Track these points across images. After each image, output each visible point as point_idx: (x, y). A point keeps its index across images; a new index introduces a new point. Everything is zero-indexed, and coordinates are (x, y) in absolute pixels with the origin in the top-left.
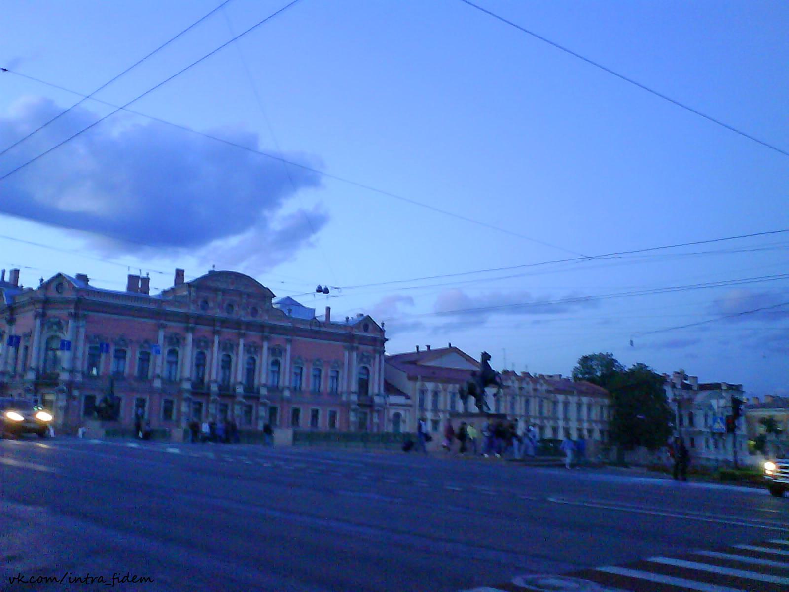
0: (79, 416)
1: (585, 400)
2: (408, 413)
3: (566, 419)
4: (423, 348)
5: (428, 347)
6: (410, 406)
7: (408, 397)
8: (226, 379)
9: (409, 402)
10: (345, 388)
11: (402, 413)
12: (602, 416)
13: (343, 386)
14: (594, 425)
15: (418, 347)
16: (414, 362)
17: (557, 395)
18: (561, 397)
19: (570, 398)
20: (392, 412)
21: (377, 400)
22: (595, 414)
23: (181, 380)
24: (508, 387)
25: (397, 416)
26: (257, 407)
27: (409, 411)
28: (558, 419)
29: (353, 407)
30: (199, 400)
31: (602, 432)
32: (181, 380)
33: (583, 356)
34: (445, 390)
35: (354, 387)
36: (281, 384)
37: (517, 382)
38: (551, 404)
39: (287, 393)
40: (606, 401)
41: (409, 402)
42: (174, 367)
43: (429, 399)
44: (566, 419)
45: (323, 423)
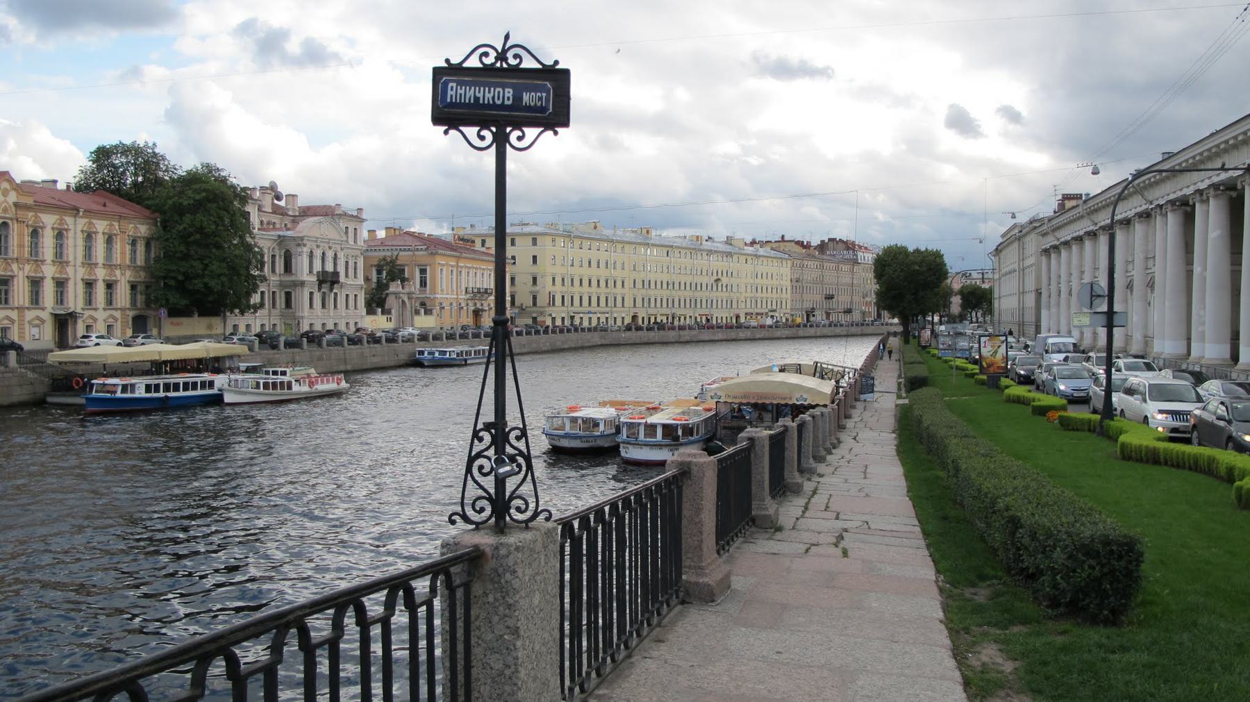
1: (101, 226)
12: (133, 259)
14: (118, 272)
18: (49, 220)
19: (69, 220)
22: (121, 251)
31: (133, 287)
40: (143, 230)
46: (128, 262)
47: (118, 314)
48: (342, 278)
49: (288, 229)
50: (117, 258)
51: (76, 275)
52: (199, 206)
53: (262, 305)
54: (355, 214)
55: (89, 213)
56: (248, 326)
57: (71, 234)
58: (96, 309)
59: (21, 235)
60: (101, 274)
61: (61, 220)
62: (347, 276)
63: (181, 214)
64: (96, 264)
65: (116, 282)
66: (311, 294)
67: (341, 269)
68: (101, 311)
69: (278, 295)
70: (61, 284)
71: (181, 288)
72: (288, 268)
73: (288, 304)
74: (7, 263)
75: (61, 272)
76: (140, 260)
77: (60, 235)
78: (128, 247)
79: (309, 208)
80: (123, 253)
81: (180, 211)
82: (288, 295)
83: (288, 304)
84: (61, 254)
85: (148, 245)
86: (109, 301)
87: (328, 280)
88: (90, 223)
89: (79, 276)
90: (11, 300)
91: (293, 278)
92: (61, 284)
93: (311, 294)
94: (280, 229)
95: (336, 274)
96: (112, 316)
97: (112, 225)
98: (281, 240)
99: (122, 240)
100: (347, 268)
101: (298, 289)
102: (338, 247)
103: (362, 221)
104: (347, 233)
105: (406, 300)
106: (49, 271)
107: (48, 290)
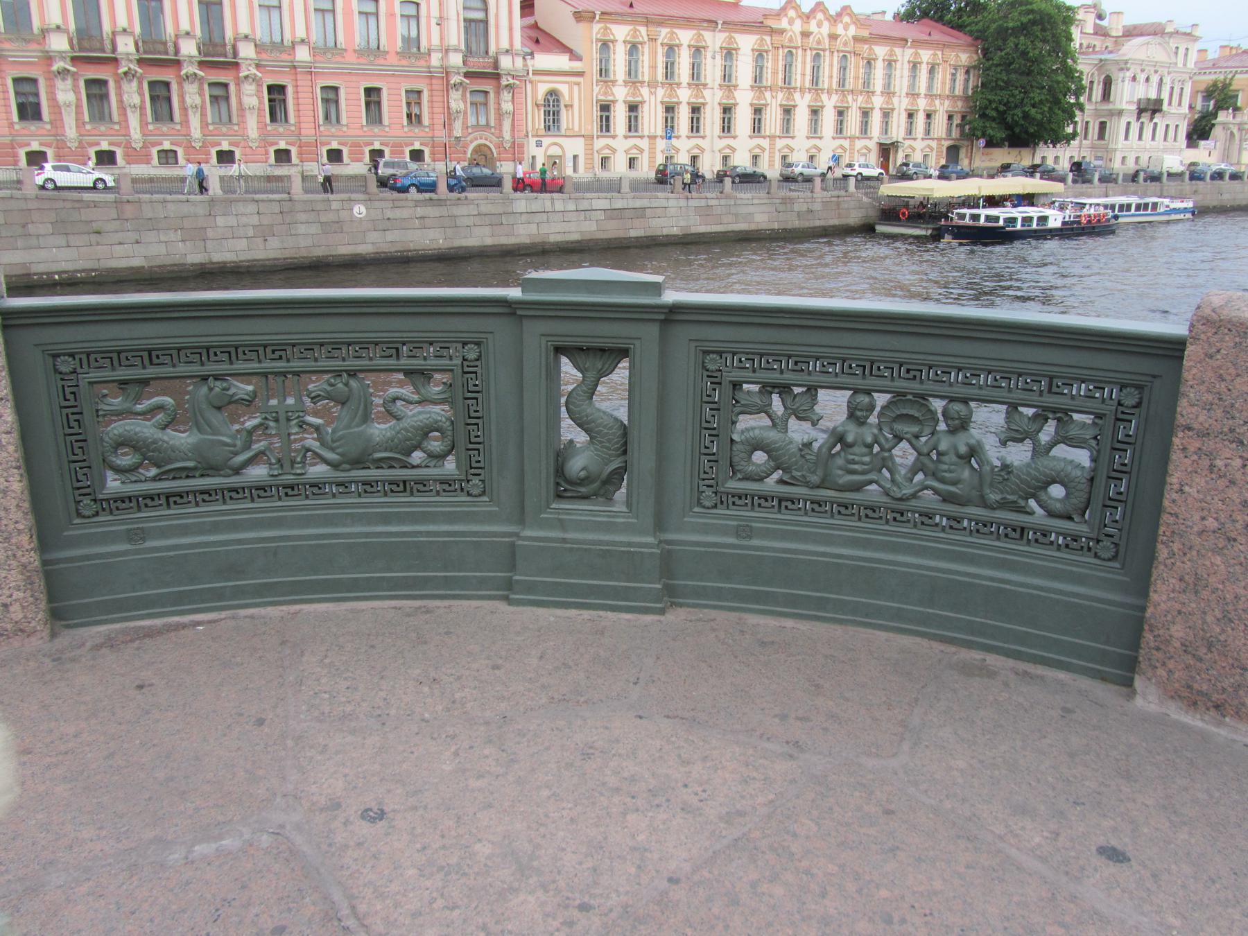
0: (11, 125)
2: (576, 88)
3: (888, 93)
6: (580, 74)
7: (574, 56)
9: (577, 66)
10: (436, 41)
11: (564, 89)
12: (953, 88)
13: (431, 37)
14: (937, 102)
17: (736, 36)
18: (881, 51)
19: (898, 51)
20: (543, 89)
21: (506, 63)
22: (942, 79)
23: (44, 32)
24: (781, 32)
26: (498, 93)
27: (578, 84)
28: (679, 84)
29: (455, 79)
30: (223, 79)
32: (44, 32)
34: (653, 40)
35: (455, 35)
36: (288, 37)
37: (826, 24)
38: (862, 63)
39: (303, 54)
41: (577, 66)
42: (275, 14)
43: (619, 57)
44: (888, 93)
47: (934, 144)
48: (1165, 107)
49: (1111, 52)
50: (938, 88)
51: (901, 104)
53: (1074, 136)
54: (1188, 31)
55: (917, 43)
56: (1057, 158)
57: (899, 65)
58: (915, 139)
59: (857, 67)
61: (635, 30)
62: (1170, 104)
63: (1005, 40)
65: (935, 111)
66: (1129, 124)
67: (1165, 96)
68: (919, 140)
69: (1091, 125)
70: (886, 114)
71: (1001, 119)
72: (1106, 96)
73: (1101, 136)
76: (958, 91)
77: (890, 64)
79: (1135, 27)
80: (943, 83)
81: (1003, 33)
82: (1103, 126)
83: (1101, 136)
85: (967, 72)
86: (928, 132)
87: (1150, 109)
88: (606, 28)
91: (1111, 107)
92: (886, 114)
93: (1129, 124)
94: (1101, 52)
95: (1159, 102)
96: (929, 146)
97: (935, 55)
98: (1102, 64)
99: (944, 71)
100: (1171, 95)
101: (1115, 119)
102: (1165, 71)
103: (1196, 39)
104: (1176, 53)
105: (1235, 131)
106: (878, 101)
107: (876, 118)
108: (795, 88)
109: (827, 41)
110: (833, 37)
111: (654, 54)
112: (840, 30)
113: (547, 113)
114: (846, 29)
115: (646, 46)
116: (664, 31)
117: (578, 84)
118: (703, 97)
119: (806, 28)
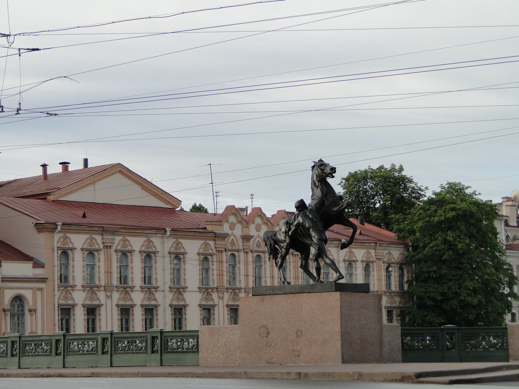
1: (78, 240)
4: (55, 169)
5: (65, 164)
6: (43, 280)
7: (38, 265)
8: (276, 260)
9: (39, 272)
11: (28, 294)
12: (389, 285)
14: (101, 295)
15: (44, 166)
16: (42, 196)
19: (156, 241)
20: (9, 295)
25: (18, 299)
28: (73, 287)
33: (350, 173)
37: (238, 227)
41: (39, 272)
44: (178, 289)
45: (109, 322)
46: (226, 285)
52: (449, 225)
60: (79, 297)
61: (92, 239)
64: (132, 288)
74: (151, 293)
75: (91, 299)
76: (394, 286)
78: (384, 273)
80: (380, 280)
84: (179, 280)
85: (401, 269)
89: (168, 302)
90: (72, 329)
106: (138, 298)
108: (98, 287)
109: (240, 241)
110: (246, 238)
111: (109, 260)
112: (252, 231)
113: (12, 316)
114: (258, 229)
115: (375, 264)
116: (118, 239)
117: (41, 289)
118: (155, 299)
119: (246, 232)
